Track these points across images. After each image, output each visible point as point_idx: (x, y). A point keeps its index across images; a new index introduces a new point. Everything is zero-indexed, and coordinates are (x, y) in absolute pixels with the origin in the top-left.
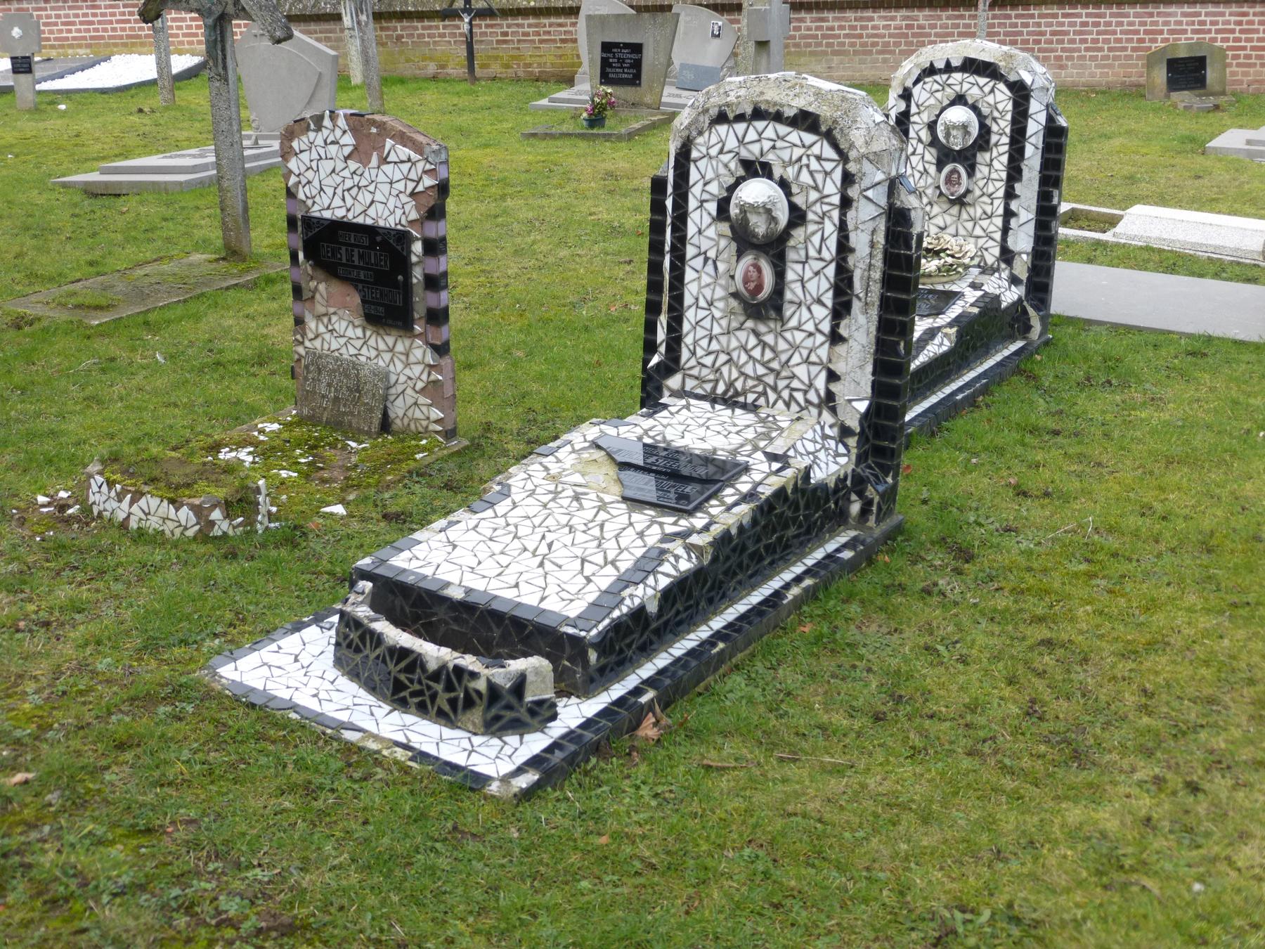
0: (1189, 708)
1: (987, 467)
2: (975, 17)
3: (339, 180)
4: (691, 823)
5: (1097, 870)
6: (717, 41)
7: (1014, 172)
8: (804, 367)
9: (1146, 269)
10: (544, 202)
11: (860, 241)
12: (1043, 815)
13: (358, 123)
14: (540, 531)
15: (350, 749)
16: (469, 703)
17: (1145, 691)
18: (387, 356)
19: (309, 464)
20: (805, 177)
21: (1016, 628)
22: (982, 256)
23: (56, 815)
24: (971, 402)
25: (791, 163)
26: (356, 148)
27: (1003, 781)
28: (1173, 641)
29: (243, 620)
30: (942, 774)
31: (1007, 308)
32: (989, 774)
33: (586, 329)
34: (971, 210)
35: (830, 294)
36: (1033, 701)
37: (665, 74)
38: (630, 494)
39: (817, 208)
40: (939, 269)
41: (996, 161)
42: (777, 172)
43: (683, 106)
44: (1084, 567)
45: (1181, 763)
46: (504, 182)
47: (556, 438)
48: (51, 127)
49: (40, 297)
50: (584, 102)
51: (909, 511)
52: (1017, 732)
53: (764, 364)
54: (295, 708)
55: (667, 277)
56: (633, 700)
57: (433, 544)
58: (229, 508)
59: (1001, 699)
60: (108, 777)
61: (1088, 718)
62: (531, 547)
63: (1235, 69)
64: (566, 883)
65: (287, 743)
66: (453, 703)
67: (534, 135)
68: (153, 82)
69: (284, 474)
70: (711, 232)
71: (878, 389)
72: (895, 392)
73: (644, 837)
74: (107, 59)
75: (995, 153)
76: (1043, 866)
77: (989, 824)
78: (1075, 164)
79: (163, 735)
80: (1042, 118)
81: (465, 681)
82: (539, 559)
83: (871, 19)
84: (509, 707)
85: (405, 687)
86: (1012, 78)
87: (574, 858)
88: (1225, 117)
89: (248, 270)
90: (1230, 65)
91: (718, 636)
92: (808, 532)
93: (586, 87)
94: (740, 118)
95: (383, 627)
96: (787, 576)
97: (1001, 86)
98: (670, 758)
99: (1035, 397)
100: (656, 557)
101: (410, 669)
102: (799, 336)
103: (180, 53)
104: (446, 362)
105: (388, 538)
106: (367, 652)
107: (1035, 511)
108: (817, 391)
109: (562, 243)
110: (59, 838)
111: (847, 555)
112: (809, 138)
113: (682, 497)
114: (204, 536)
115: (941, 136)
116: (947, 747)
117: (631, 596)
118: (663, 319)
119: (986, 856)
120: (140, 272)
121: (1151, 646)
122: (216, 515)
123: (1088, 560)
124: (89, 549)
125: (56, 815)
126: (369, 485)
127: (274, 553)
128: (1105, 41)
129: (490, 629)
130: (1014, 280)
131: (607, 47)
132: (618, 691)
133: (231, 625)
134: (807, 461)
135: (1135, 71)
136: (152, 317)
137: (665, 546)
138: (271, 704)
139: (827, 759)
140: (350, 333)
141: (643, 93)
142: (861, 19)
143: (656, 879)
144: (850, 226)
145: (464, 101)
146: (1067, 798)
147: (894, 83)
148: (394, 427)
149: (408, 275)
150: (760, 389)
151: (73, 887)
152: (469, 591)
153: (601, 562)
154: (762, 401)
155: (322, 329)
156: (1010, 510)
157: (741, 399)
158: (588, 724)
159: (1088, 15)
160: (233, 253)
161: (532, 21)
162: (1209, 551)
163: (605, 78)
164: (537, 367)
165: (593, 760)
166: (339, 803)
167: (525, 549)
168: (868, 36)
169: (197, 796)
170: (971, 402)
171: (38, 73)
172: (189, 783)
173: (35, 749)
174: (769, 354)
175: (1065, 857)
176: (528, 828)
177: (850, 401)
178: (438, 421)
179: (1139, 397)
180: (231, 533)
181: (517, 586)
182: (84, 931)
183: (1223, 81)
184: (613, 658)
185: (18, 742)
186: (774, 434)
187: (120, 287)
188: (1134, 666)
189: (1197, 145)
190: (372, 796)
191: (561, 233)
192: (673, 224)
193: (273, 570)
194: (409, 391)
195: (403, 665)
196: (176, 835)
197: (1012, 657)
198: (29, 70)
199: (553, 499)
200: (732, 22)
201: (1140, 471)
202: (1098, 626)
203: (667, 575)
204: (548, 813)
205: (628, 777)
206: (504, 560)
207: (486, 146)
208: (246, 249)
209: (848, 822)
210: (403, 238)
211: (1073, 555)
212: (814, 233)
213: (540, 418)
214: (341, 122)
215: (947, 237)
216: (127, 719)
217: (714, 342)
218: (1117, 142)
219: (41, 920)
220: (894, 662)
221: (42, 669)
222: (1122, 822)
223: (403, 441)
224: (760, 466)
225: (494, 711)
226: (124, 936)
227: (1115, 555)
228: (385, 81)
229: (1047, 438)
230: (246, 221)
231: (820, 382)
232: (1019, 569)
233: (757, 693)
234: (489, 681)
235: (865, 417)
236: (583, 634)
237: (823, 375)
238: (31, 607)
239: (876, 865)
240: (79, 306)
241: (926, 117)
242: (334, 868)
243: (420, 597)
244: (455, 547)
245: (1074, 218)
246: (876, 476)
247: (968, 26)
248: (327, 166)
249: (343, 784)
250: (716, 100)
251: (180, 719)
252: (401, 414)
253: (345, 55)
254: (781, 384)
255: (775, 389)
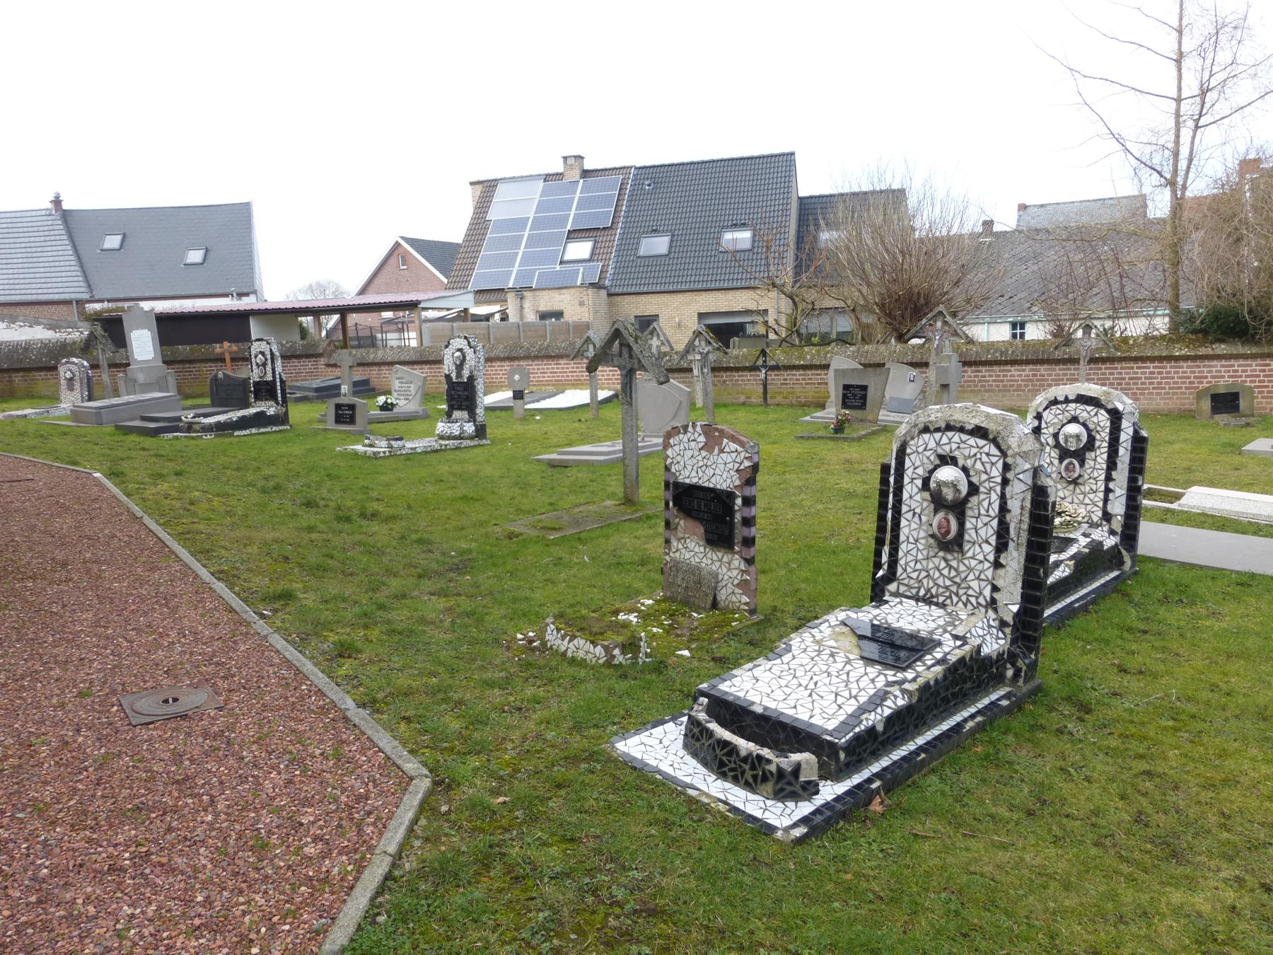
0: (1258, 830)
1: (1098, 651)
2: (1078, 369)
3: (695, 461)
4: (906, 872)
5: (1197, 940)
6: (912, 384)
7: (1112, 464)
8: (977, 582)
9: (1203, 528)
10: (808, 476)
11: (1014, 505)
12: (1152, 894)
13: (708, 430)
14: (810, 674)
15: (691, 801)
16: (765, 779)
17: (1223, 814)
18: (718, 564)
19: (669, 625)
20: (979, 466)
21: (1124, 761)
22: (1090, 517)
23: (520, 825)
24: (1084, 609)
25: (969, 457)
26: (706, 444)
27: (1121, 867)
28: (1242, 781)
29: (630, 716)
30: (1077, 857)
31: (1108, 550)
32: (1110, 860)
33: (834, 552)
34: (1082, 487)
35: (994, 537)
36: (1140, 813)
37: (881, 403)
38: (866, 655)
39: (986, 484)
40: (1061, 524)
41: (1100, 457)
42: (961, 462)
43: (901, 423)
44: (1171, 723)
45: (1256, 869)
46: (784, 464)
47: (816, 618)
48: (532, 428)
49: (522, 522)
50: (832, 418)
51: (1045, 677)
52: (1129, 833)
53: (950, 579)
54: (659, 772)
55: (889, 523)
56: (867, 786)
57: (745, 678)
58: (624, 648)
59: (1116, 808)
60: (551, 804)
61: (1181, 829)
62: (804, 684)
63: (1260, 400)
64: (825, 903)
65: (654, 793)
66: (755, 777)
67: (802, 437)
68: (587, 405)
69: (655, 630)
70: (918, 497)
71: (1026, 598)
72: (1037, 601)
73: (875, 878)
74: (563, 392)
75: (1098, 453)
76: (1155, 931)
77: (1113, 896)
78: (1152, 459)
79: (583, 781)
80: (1131, 431)
81: (763, 764)
82: (809, 691)
83: (1010, 371)
84: (789, 783)
85: (726, 765)
86: (1110, 406)
87: (830, 887)
88: (1255, 431)
89: (636, 511)
90: (1257, 397)
91: (921, 749)
92: (979, 686)
93: (833, 410)
94: (938, 430)
95: (714, 726)
96: (965, 714)
97: (1102, 411)
98: (891, 826)
99: (1129, 608)
100: (879, 698)
101: (730, 754)
102: (973, 563)
103: (603, 389)
104: (752, 569)
105: (715, 672)
106: (704, 741)
107: (1134, 684)
108: (985, 597)
109: (819, 501)
110: (522, 839)
111: (1005, 703)
112: (981, 442)
113: (898, 659)
114: (609, 664)
115: (1062, 442)
116: (1079, 838)
117: (867, 719)
118: (886, 549)
119: (1112, 919)
120: (577, 510)
121: (1225, 782)
122: (617, 652)
123: (1173, 719)
124: (544, 667)
125: (520, 825)
126: (704, 640)
127: (648, 677)
128: (1166, 383)
129: (778, 733)
130: (1112, 532)
131: (846, 387)
132: (857, 779)
133: (623, 718)
134: (978, 641)
135: (1189, 402)
136: (583, 536)
137: (888, 689)
138: (646, 768)
139: (996, 838)
140: (697, 549)
141: (867, 414)
142: (1003, 371)
143: (883, 907)
144: (1008, 496)
145: (761, 417)
146: (1170, 884)
147: (1030, 410)
148: (720, 606)
149: (732, 517)
150: (947, 594)
151: (528, 871)
152: (766, 708)
153: (848, 696)
154: (948, 602)
155: (680, 546)
156: (1115, 681)
157: (935, 600)
158: (838, 799)
159: (1154, 367)
160: (629, 501)
161: (801, 372)
162: (1265, 719)
163: (845, 405)
164: (805, 574)
165: (842, 823)
166: (684, 835)
167: (800, 685)
168: (1008, 381)
169: (601, 821)
170: (1084, 609)
171: (527, 399)
172: (597, 813)
173: (511, 782)
174: (953, 573)
175: (1171, 927)
176: (800, 863)
177: (1006, 605)
178: (746, 604)
179: (1203, 612)
180: (624, 663)
181: (795, 707)
182: (533, 899)
183: (1252, 407)
184: (855, 758)
185: (501, 778)
186: (957, 623)
187: (566, 518)
188: (1213, 795)
189: (1236, 449)
190: (704, 833)
191: (819, 495)
192: (894, 492)
193: (647, 687)
194: (730, 585)
195: (725, 751)
196: (588, 844)
197: (1123, 781)
198: (522, 398)
199: (818, 655)
200: (922, 373)
201: (1208, 661)
202: (1184, 765)
203: (890, 708)
204: (815, 855)
205: (864, 836)
206: (788, 691)
207: (774, 443)
208: (636, 499)
209: (1012, 883)
210: (730, 495)
211: (1163, 715)
212: (984, 500)
213: (806, 605)
214: (699, 429)
215: (1067, 504)
216: (563, 770)
217: (918, 564)
218: (1177, 446)
219: (509, 888)
220: (1040, 777)
221: (516, 735)
222: (1213, 906)
223: (724, 614)
224: (948, 643)
225: (780, 786)
226: (556, 905)
227: (1193, 717)
228: (716, 405)
229: (1139, 635)
230: (637, 483)
231: (987, 592)
232: (1124, 721)
233: (947, 789)
234: (778, 765)
235: (1017, 615)
236: (836, 741)
237: (989, 588)
238: (512, 699)
239: (1033, 916)
240: (543, 528)
241: (1051, 430)
242: (681, 876)
243: (736, 709)
244: (758, 680)
245: (1151, 494)
246: (1024, 654)
247: (1074, 375)
248: (689, 453)
249: (687, 822)
250: (922, 420)
251: (593, 773)
252: (724, 598)
253: (694, 391)
254: (961, 592)
255: (957, 594)
